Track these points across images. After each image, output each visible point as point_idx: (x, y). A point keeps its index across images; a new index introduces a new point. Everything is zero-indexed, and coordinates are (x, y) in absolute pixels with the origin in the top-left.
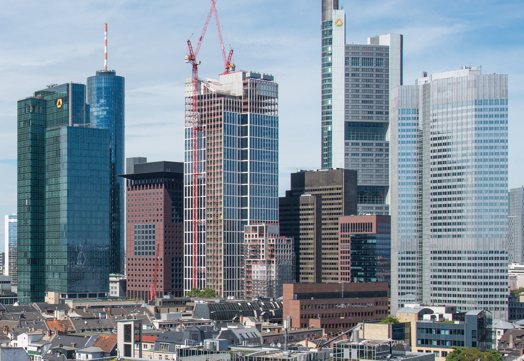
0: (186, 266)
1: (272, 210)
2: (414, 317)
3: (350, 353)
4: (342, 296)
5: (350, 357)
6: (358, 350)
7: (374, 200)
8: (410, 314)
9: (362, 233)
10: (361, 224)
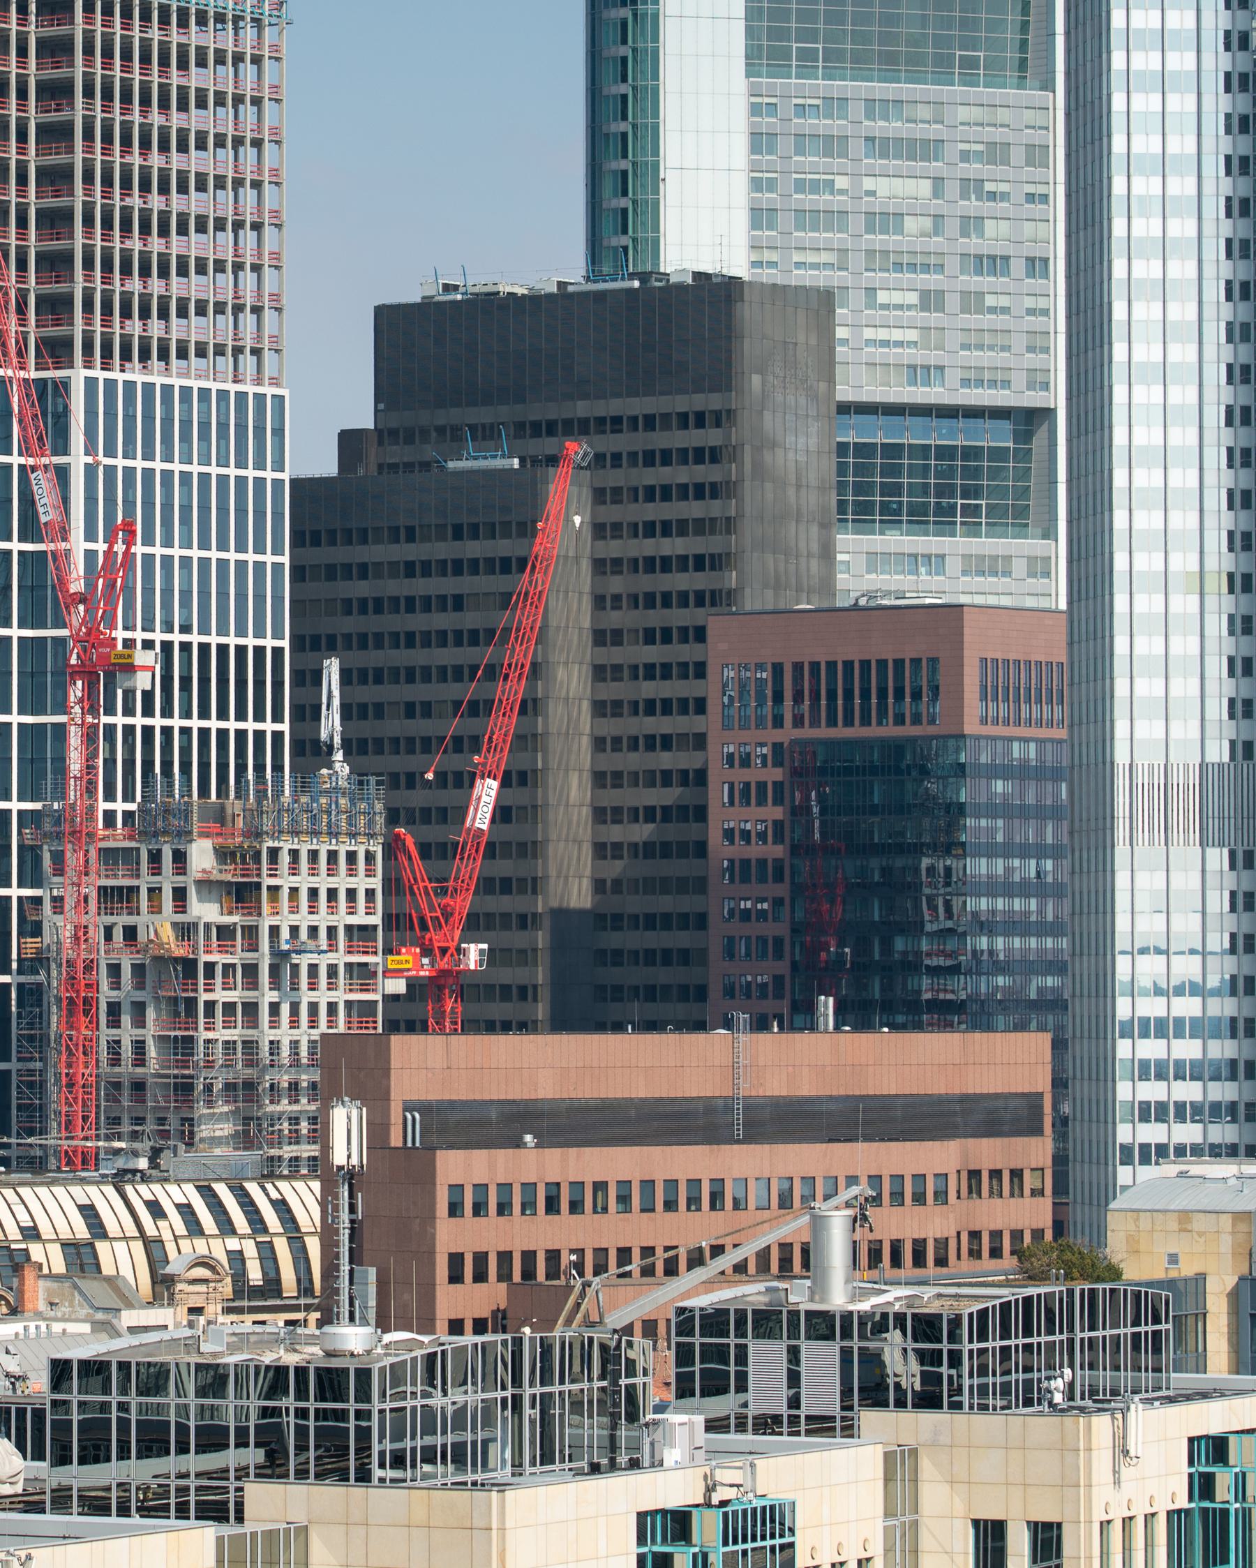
0: (277, 736)
1: (148, 474)
2: (1226, 1243)
3: (794, 1379)
4: (739, 1132)
5: (794, 1354)
6: (846, 1354)
7: (952, 510)
8: (1199, 1223)
9: (874, 731)
10: (831, 665)
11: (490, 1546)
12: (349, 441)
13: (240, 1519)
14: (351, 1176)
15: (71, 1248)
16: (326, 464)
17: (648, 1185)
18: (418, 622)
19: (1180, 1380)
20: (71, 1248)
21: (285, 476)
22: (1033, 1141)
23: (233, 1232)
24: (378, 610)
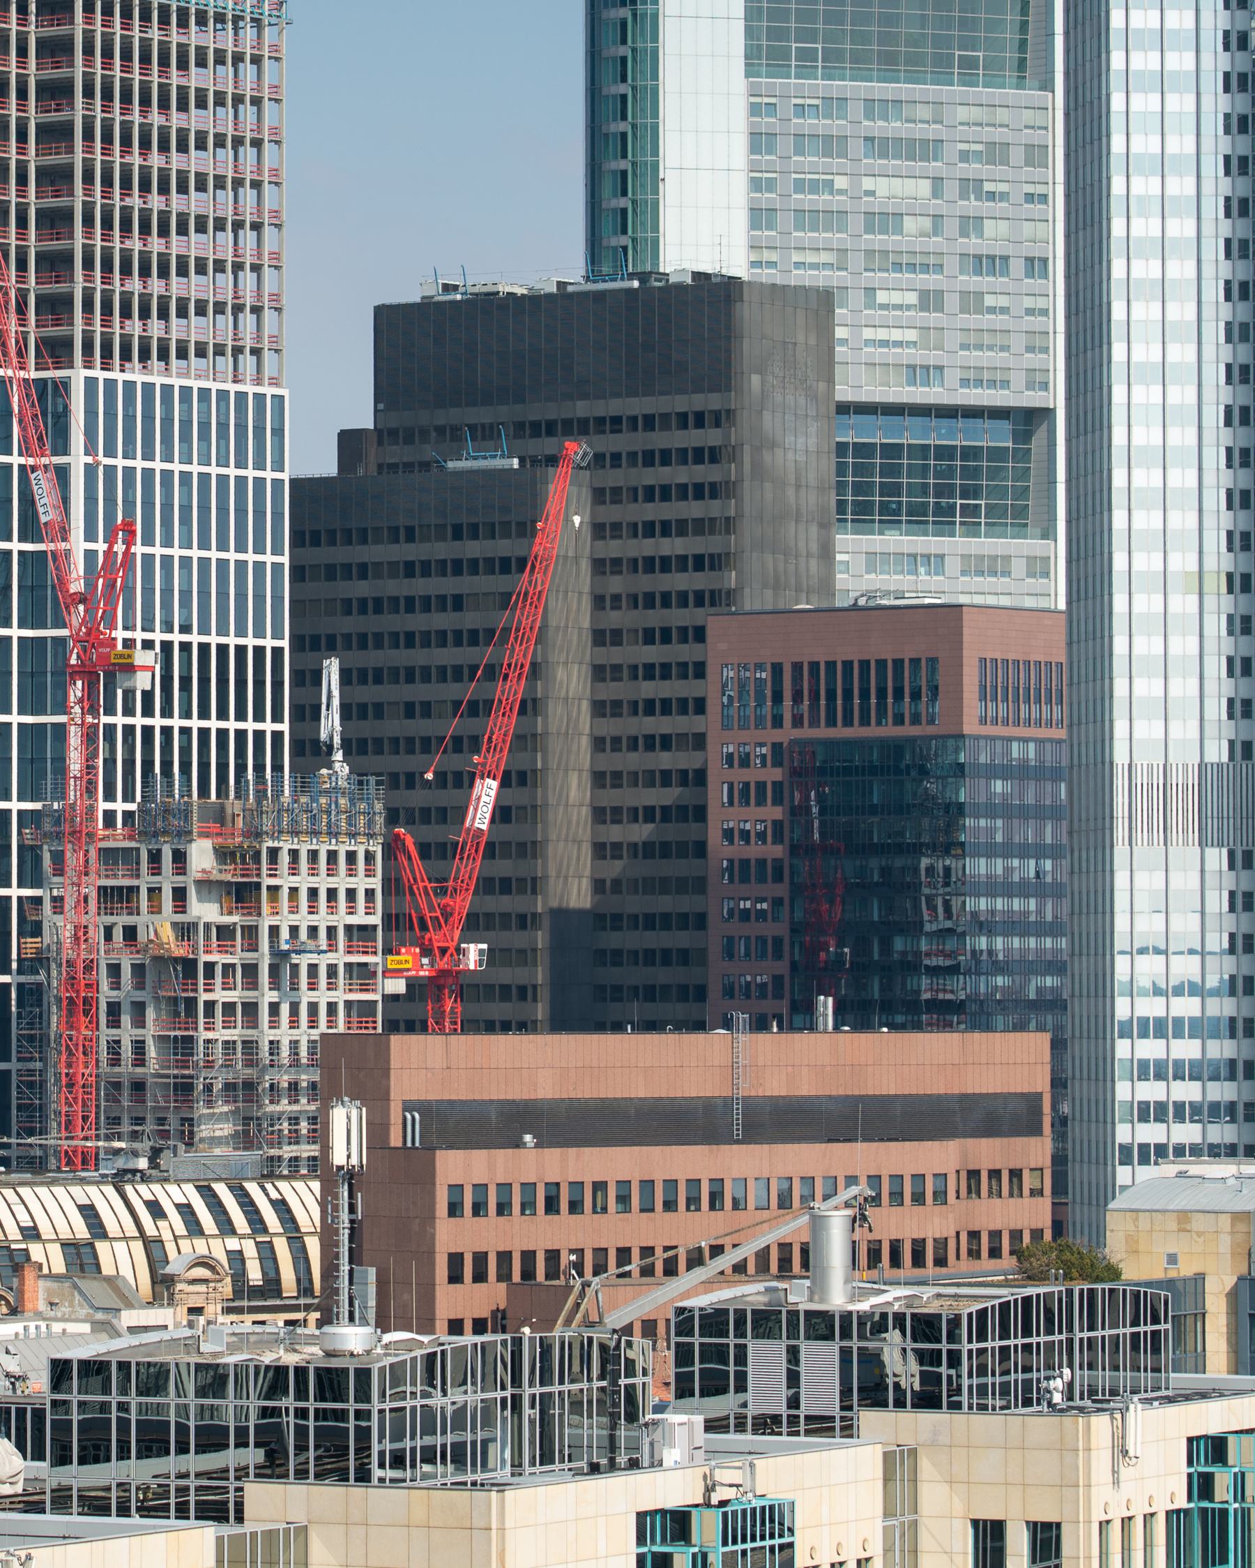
0: (277, 736)
1: (148, 474)
2: (1225, 1243)
3: (793, 1379)
4: (738, 1132)
5: (793, 1354)
6: (845, 1354)
7: (951, 510)
8: (1198, 1223)
9: (873, 731)
10: (831, 665)
11: (490, 1546)
12: (349, 441)
13: (240, 1519)
14: (351, 1176)
15: (71, 1248)
16: (326, 464)
17: (648, 1185)
18: (418, 622)
19: (1179, 1380)
20: (71, 1248)
21: (285, 476)
22: (1033, 1141)
23: (233, 1232)
24: (378, 610)
